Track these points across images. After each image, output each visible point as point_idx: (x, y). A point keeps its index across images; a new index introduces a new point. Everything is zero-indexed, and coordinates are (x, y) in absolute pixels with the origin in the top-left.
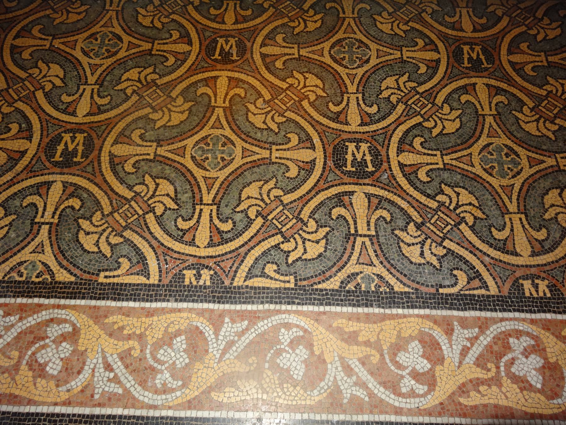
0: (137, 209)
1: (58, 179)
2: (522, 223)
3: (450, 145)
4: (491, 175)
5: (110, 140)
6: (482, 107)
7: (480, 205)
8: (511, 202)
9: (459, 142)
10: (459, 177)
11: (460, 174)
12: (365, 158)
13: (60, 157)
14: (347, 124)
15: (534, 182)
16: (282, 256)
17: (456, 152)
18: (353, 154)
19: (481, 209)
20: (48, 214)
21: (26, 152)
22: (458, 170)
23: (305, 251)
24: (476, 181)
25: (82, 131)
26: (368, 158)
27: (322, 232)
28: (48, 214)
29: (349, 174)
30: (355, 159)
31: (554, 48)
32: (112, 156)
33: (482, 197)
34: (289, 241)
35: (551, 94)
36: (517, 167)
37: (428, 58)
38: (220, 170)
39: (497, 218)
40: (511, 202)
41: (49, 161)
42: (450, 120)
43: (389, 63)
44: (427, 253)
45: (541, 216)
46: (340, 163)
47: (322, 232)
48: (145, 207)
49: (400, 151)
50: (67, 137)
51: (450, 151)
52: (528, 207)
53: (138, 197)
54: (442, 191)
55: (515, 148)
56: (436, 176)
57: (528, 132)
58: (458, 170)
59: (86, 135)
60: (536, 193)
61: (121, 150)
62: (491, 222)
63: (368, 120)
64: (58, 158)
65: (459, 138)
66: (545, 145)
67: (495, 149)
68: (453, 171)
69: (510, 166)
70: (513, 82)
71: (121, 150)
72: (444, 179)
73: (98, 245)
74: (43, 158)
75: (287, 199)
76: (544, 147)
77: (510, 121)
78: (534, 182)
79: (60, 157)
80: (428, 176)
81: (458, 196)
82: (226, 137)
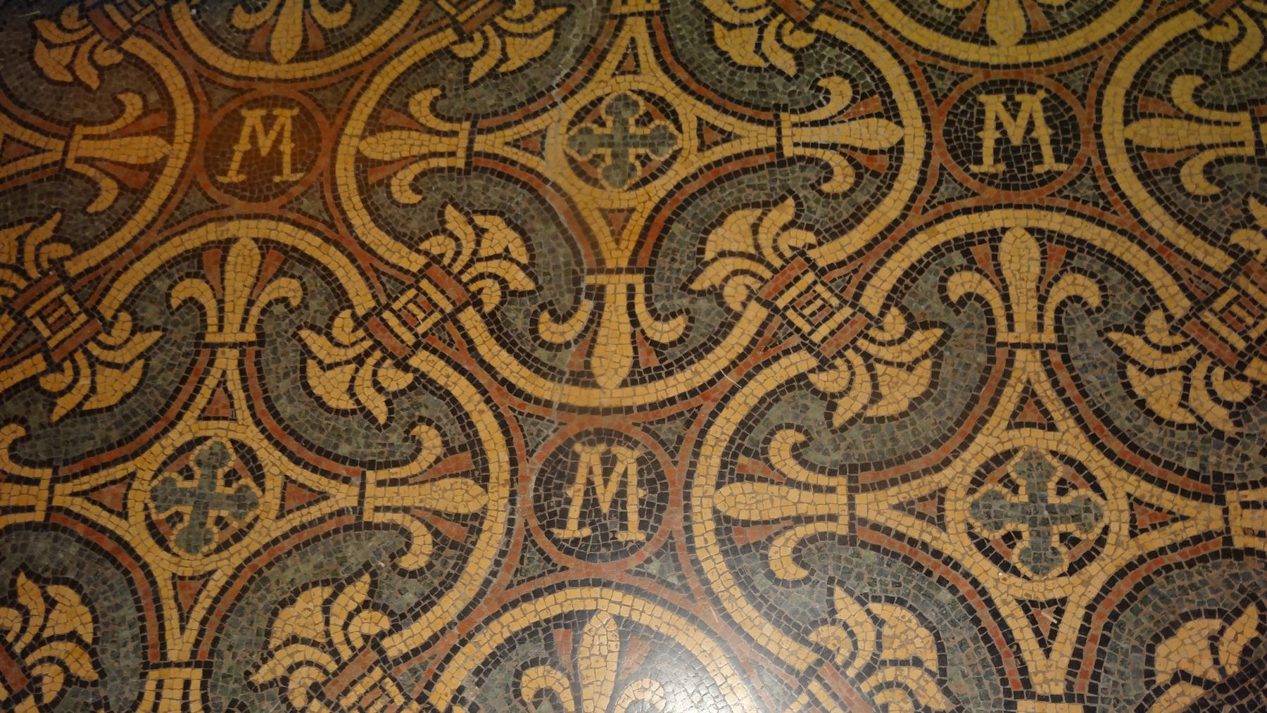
0: (437, 297)
1: (246, 231)
2: (185, 696)
3: (89, 446)
4: (162, 542)
5: (356, 125)
6: (221, 320)
7: (95, 641)
8: (182, 629)
9: (115, 436)
10: (74, 549)
11: (79, 540)
12: (1034, 135)
13: (239, 172)
14: (987, 41)
15: (269, 566)
16: (817, 411)
17: (95, 469)
18: (999, 126)
19: (93, 654)
20: (233, 320)
21: (164, 165)
22: (80, 529)
23: (876, 397)
24: (114, 561)
25: (287, 103)
26: (1043, 133)
27: (923, 340)
28: (233, 320)
29: (989, 179)
30: (1003, 141)
31: (506, 104)
32: (363, 164)
33: (111, 615)
34: (833, 367)
35: (435, 269)
36: (238, 517)
37: (133, 161)
38: (636, 186)
39: (124, 680)
40: (182, 629)
41: (214, 182)
42: (118, 366)
43: (22, 181)
44: (1199, 397)
45: (248, 674)
46: (967, 151)
47: (923, 340)
48: (455, 291)
49: (1132, 112)
50: (253, 117)
51: (78, 467)
52: (222, 646)
53: (435, 266)
54: (1251, 218)
55: (261, 454)
56: (14, 549)
57: (318, 399)
58: (80, 529)
59: (296, 111)
60: (260, 599)
61: (383, 147)
62: (102, 693)
63: (1043, 23)
64: (234, 176)
65: (118, 425)
66: (349, 441)
67: (204, 458)
68: (65, 530)
69: (224, 513)
70: (342, 229)
71: (383, 147)
72: (31, 558)
73: (353, 395)
74: (203, 179)
75: (826, 254)
76: (344, 450)
77: (284, 362)
78: (269, 566)
79: (239, 172)
80: (1210, 180)
81: (48, 612)
82: (649, 97)
